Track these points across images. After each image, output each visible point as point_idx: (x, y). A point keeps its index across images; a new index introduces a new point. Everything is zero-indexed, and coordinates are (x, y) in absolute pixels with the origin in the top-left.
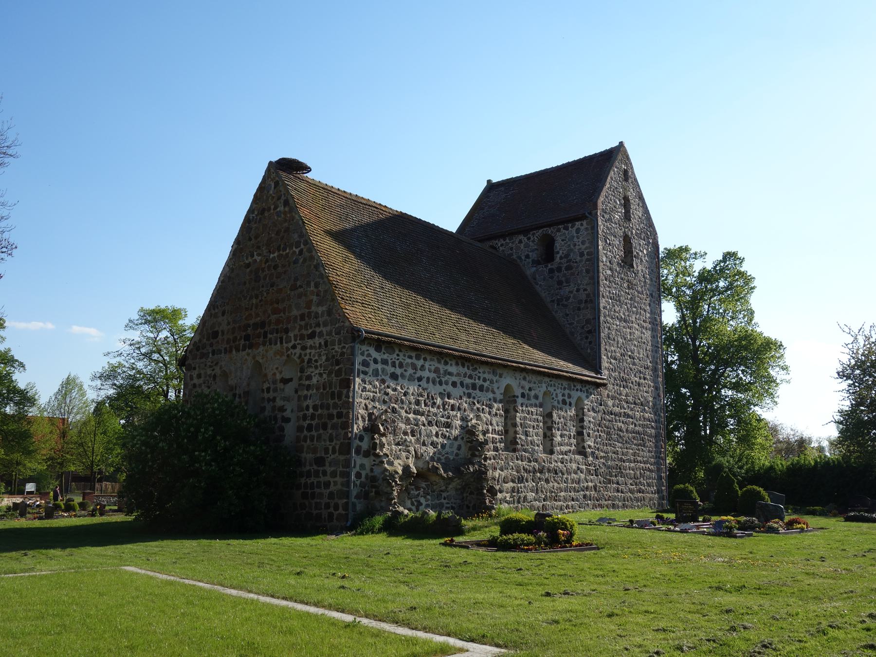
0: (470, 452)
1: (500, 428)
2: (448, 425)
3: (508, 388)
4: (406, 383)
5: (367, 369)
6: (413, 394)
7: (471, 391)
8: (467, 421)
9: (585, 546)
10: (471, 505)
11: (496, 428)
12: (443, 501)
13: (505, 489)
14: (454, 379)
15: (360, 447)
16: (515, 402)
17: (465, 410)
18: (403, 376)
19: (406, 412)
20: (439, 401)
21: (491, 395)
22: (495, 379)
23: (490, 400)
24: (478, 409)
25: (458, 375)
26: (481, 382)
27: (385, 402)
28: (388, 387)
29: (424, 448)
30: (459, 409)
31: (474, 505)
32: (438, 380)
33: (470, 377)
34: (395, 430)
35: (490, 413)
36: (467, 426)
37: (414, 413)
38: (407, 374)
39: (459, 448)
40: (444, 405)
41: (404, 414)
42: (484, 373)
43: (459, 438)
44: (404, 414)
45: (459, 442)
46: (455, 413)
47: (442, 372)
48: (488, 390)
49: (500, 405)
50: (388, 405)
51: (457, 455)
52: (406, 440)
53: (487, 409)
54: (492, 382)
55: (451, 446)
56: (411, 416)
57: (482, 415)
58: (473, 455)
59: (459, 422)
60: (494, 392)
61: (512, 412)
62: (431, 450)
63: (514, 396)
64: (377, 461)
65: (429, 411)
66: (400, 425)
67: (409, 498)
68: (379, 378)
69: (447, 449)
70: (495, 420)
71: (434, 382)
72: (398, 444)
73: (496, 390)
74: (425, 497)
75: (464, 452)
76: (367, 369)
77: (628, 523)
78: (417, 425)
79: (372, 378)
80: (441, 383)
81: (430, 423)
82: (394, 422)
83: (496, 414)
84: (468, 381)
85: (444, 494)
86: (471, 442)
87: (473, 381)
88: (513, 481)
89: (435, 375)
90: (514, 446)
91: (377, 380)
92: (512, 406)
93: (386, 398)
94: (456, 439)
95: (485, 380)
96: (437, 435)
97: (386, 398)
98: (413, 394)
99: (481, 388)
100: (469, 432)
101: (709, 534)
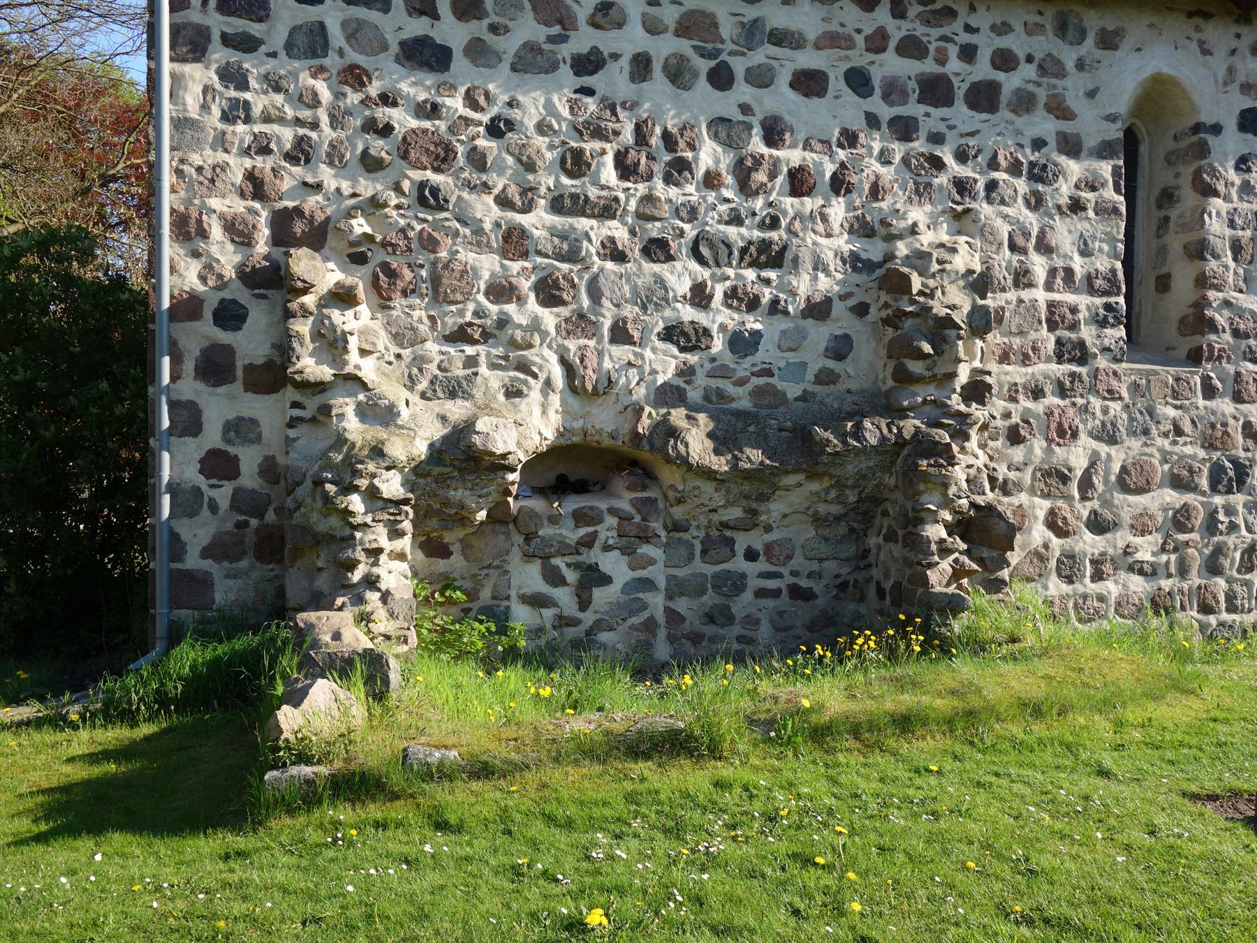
0: (891, 365)
1: (1102, 264)
2: (769, 257)
3: (1157, 97)
4: (497, 86)
5: (256, 29)
6: (542, 128)
7: (913, 109)
8: (891, 238)
9: (19, 814)
10: (888, 585)
11: (1079, 265)
12: (739, 564)
13: (1126, 516)
14: (808, 59)
15: (229, 350)
16: (1203, 151)
17: (876, 192)
18: (478, 52)
19: (504, 202)
20: (709, 154)
21: (1047, 126)
22: (1069, 57)
23: (1038, 144)
24: (962, 186)
25: (832, 40)
26: (982, 70)
27: (371, 164)
28: (387, 99)
29: (623, 352)
30: (839, 185)
31: (897, 586)
32: (704, 66)
33: (912, 48)
34: (435, 280)
35: (1036, 202)
36: (890, 257)
37: (557, 206)
38: (510, 45)
39: (841, 348)
40: (743, 173)
41: (486, 210)
42: (1002, 29)
43: (838, 308)
44: (486, 210)
45: (842, 321)
46: (810, 204)
47: (727, 29)
48: (1024, 102)
49: (1105, 169)
50: (390, 175)
51: (826, 377)
52: (503, 322)
53: (1022, 185)
54: (1050, 67)
55: (791, 342)
56: (539, 221)
57: (985, 210)
58: (904, 378)
59: (843, 243)
60: (1059, 110)
61: (1189, 198)
62: (665, 363)
63: (1197, 128)
64: (312, 404)
65: (649, 199)
66: (467, 256)
67: (528, 557)
68: (332, 61)
69: (766, 353)
70: (1064, 234)
71: (678, 74)
72: (460, 336)
73: (1074, 100)
74: (627, 551)
75: (867, 364)
76: (256, 29)
77: (591, 378)
78: (572, 256)
79: (283, 65)
80: (721, 78)
81: (657, 250)
82: (430, 244)
83: (1076, 206)
84: (891, 65)
85: (742, 541)
86: (895, 319)
87: (929, 66)
88: (1178, 483)
89: (684, 46)
90: (1195, 340)
91: (317, 72)
92: (1187, 171)
93: (379, 147)
94: (818, 310)
95: (1005, 61)
96: (700, 296)
97: (379, 147)
98: (542, 128)
99: (984, 98)
100: (883, 279)
101: (41, 838)
